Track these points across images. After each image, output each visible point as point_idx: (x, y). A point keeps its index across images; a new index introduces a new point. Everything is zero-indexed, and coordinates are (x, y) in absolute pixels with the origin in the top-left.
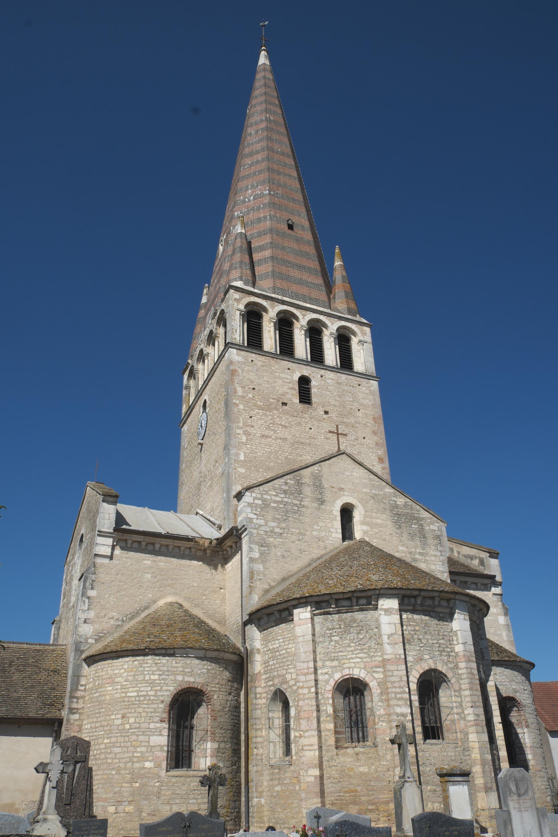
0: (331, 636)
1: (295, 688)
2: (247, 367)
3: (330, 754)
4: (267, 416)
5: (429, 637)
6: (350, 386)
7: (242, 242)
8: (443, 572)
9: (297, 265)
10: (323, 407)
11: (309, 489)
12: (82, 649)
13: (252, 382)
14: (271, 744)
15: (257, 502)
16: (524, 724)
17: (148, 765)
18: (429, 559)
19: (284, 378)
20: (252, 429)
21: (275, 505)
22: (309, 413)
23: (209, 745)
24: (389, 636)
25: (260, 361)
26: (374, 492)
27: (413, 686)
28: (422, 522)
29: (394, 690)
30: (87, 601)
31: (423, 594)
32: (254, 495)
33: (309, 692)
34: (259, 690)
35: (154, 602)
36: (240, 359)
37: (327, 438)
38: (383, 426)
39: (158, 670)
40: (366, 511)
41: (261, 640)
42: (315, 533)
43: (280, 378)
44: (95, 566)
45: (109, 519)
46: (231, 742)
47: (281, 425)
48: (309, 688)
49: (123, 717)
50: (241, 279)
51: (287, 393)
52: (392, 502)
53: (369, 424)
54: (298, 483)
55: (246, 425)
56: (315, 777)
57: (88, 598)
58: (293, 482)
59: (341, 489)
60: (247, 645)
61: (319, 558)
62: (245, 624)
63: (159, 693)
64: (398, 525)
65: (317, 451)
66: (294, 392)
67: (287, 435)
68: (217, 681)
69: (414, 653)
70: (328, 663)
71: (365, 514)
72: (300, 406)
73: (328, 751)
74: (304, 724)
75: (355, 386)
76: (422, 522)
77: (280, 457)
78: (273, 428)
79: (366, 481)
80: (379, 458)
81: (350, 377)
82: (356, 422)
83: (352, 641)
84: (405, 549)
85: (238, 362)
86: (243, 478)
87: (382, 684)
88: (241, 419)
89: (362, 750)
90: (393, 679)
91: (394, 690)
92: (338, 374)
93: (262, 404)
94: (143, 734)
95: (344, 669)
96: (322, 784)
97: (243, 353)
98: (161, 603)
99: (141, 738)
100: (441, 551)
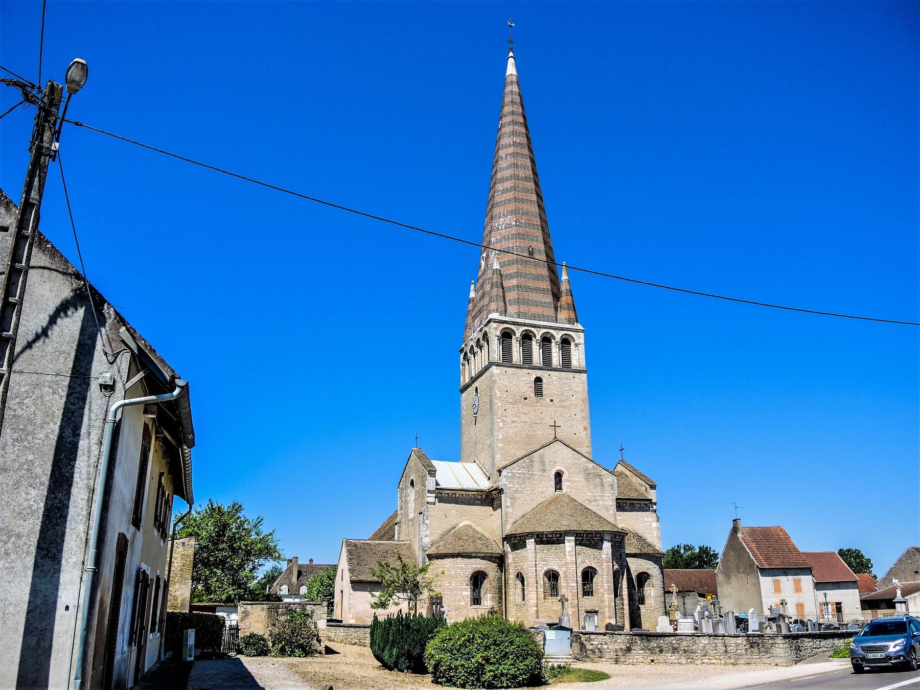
1: (527, 572)
3: (541, 602)
5: (589, 551)
11: (537, 464)
16: (651, 585)
17: (462, 603)
23: (488, 595)
24: (569, 552)
26: (574, 461)
27: (579, 574)
32: (507, 471)
33: (533, 575)
34: (511, 571)
35: (458, 525)
38: (588, 405)
42: (540, 489)
51: (527, 391)
56: (535, 611)
57: (426, 524)
59: (555, 462)
61: (542, 503)
64: (587, 480)
66: (531, 389)
69: (581, 559)
70: (541, 562)
72: (535, 399)
73: (540, 600)
74: (530, 589)
79: (570, 456)
84: (591, 494)
87: (565, 573)
96: (537, 613)
98: (461, 525)
99: (458, 592)
100: (612, 494)
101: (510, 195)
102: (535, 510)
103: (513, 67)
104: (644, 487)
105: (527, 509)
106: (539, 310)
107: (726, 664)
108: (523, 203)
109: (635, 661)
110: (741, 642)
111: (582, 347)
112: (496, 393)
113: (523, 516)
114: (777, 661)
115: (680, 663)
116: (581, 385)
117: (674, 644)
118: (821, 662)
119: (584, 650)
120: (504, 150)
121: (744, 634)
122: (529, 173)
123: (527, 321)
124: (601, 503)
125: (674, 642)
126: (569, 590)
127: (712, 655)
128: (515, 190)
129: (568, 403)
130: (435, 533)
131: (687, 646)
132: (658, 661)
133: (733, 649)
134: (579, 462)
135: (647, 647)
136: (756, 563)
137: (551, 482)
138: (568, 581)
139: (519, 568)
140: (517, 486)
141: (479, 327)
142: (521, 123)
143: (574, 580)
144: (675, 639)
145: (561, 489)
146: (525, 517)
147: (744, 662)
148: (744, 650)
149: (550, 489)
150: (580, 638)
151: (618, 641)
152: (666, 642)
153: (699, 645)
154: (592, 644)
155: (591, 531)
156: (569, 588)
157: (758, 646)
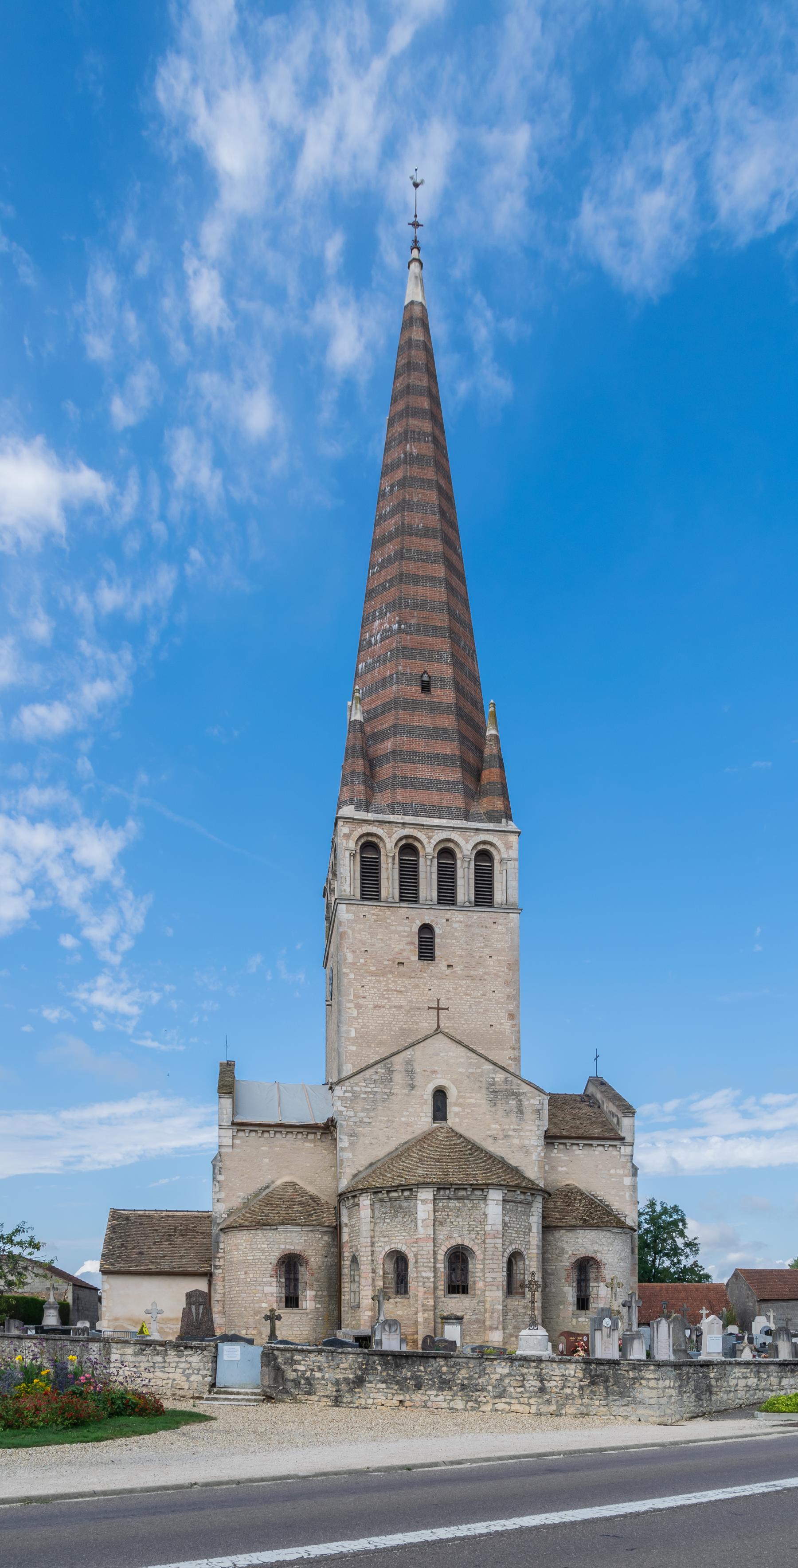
0: (385, 1218)
2: (359, 926)
4: (379, 982)
6: (482, 927)
7: (355, 738)
8: (538, 1146)
9: (428, 757)
10: (446, 960)
12: (218, 1222)
13: (364, 943)
14: (352, 1293)
15: (347, 1094)
18: (524, 1134)
19: (401, 931)
20: (364, 1000)
21: (365, 1096)
25: (374, 914)
26: (470, 1070)
27: (441, 1257)
28: (521, 1097)
29: (422, 1260)
30: (217, 1184)
32: (344, 1088)
35: (273, 1182)
36: (350, 916)
37: (448, 999)
39: (267, 1241)
40: (459, 1092)
42: (403, 1119)
43: (396, 932)
44: (220, 1156)
45: (227, 1114)
47: (396, 991)
49: (246, 1273)
50: (351, 802)
51: (404, 950)
52: (489, 1080)
53: (501, 974)
54: (389, 1071)
55: (357, 996)
56: (369, 1316)
57: (218, 1182)
58: (383, 1071)
59: (434, 1072)
61: (406, 1143)
63: (268, 1257)
66: (412, 947)
67: (403, 1002)
68: (313, 1248)
69: (445, 1233)
70: (382, 1239)
71: (458, 1096)
76: (521, 1097)
77: (394, 1028)
78: (386, 996)
79: (462, 1060)
80: (509, 1014)
81: (484, 914)
82: (485, 973)
83: (398, 1223)
85: (348, 920)
86: (354, 1056)
91: (422, 1260)
92: (469, 914)
93: (375, 969)
94: (259, 1285)
97: (353, 908)
98: (279, 1182)
99: (258, 1288)
100: (539, 1125)
105: (380, 1152)
106: (433, 797)
107: (539, 1414)
108: (416, 583)
109: (370, 1401)
111: (512, 866)
113: (371, 1165)
114: (642, 1411)
117: (444, 1374)
118: (741, 1418)
119: (281, 1381)
122: (434, 520)
123: (408, 819)
124: (516, 1141)
125: (444, 1369)
126: (421, 1284)
129: (481, 971)
130: (233, 1195)
131: (467, 1378)
132: (412, 1404)
133: (556, 1387)
134: (479, 1071)
135: (394, 1377)
137: (425, 1107)
138: (420, 1269)
140: (361, 1115)
142: (424, 411)
143: (430, 1267)
144: (446, 1365)
145: (444, 1118)
146: (374, 1167)
149: (423, 1119)
150: (276, 1359)
151: (342, 1366)
153: (492, 1376)
154: (295, 1370)
156: (421, 1279)
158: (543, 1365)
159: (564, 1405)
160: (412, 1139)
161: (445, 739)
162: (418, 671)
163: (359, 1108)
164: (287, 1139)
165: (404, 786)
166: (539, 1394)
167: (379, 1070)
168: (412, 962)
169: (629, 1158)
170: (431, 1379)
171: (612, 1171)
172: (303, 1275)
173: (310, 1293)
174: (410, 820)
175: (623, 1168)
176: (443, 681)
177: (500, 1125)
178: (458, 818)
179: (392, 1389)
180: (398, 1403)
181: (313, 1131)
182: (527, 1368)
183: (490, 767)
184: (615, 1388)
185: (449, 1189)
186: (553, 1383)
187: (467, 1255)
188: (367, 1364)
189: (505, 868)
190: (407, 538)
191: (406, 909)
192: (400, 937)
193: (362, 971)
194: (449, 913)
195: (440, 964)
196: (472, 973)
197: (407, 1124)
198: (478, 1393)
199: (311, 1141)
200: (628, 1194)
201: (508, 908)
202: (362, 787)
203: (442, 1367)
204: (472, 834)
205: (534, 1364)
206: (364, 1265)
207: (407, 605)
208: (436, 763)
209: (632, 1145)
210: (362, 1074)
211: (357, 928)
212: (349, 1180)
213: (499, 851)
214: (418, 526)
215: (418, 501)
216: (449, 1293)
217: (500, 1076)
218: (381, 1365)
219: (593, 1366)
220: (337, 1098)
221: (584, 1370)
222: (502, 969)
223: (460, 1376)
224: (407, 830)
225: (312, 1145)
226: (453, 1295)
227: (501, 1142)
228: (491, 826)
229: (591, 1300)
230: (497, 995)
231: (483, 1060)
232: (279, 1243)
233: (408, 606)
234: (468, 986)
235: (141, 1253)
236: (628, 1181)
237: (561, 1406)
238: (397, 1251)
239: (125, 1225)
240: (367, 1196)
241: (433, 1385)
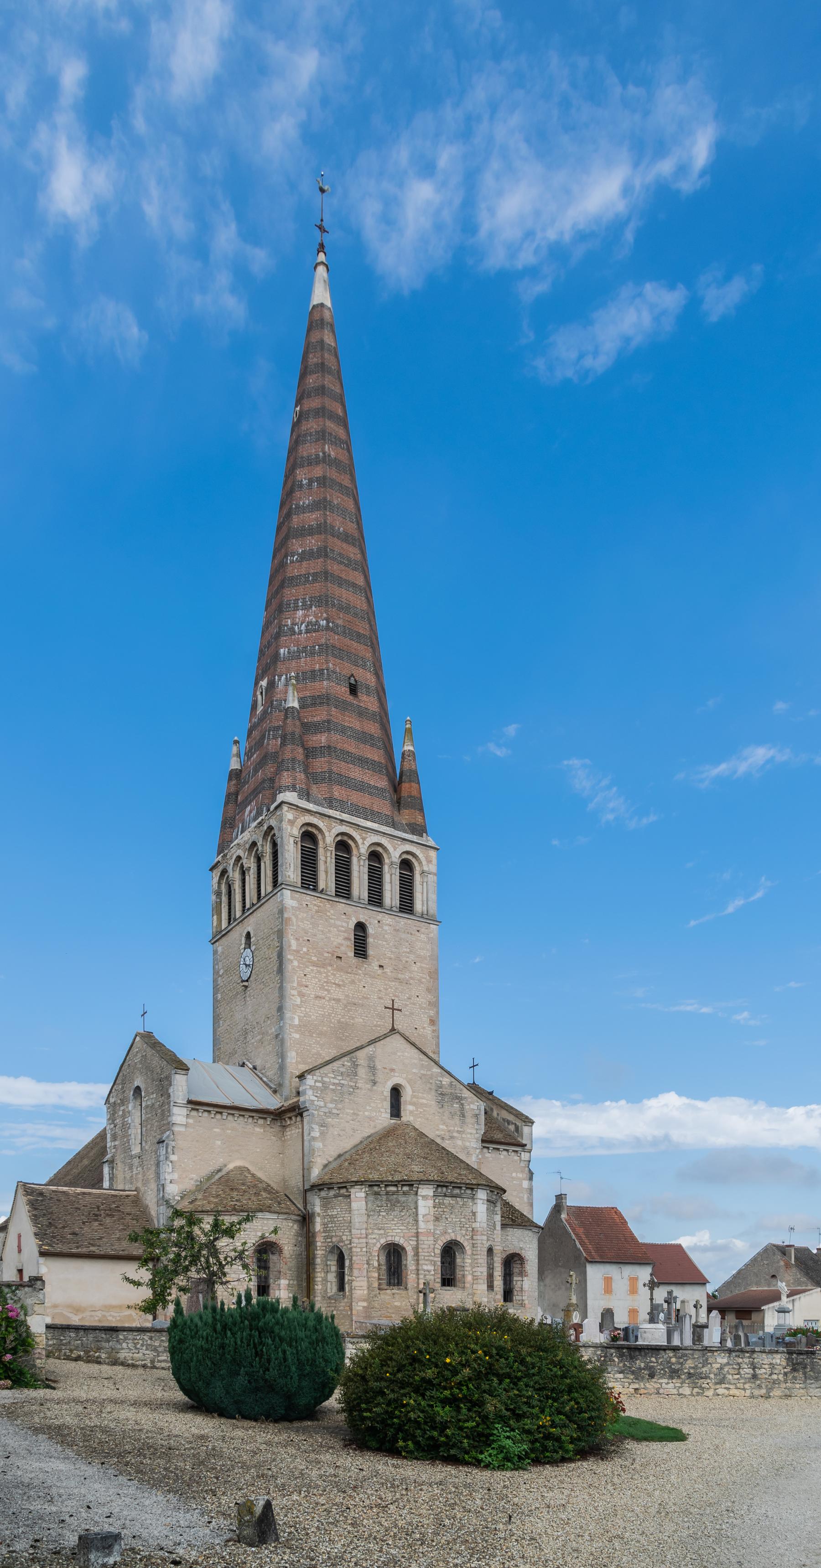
0: (380, 1211)
1: (349, 1246)
3: (374, 1293)
8: (477, 1148)
9: (359, 759)
19: (340, 926)
20: (306, 989)
22: (364, 969)
26: (422, 1072)
30: (170, 1164)
31: (453, 1185)
32: (315, 1078)
34: (319, 1244)
35: (225, 1166)
37: (380, 998)
40: (413, 1092)
41: (321, 1206)
42: (366, 1113)
46: (297, 1280)
47: (335, 984)
48: (361, 1248)
51: (342, 945)
53: (423, 980)
54: (354, 1065)
55: (300, 984)
56: (364, 1307)
58: (349, 1064)
59: (392, 1070)
60: (308, 1207)
61: (369, 1137)
62: (306, 1191)
64: (441, 1104)
65: (370, 1013)
68: (286, 1236)
70: (376, 1231)
72: (355, 961)
74: (356, 1272)
75: (413, 933)
77: (333, 1020)
78: (326, 988)
79: (416, 1061)
80: (430, 1020)
81: (409, 922)
82: (411, 978)
83: (395, 1217)
86: (297, 1044)
87: (416, 1249)
88: (296, 978)
89: (397, 1291)
90: (423, 1246)
92: (397, 918)
93: (316, 959)
95: (388, 1236)
97: (297, 895)
98: (231, 1166)
100: (477, 1129)
101: (315, 566)
102: (359, 1147)
103: (325, 289)
104: (514, 1126)
105: (347, 1144)
106: (364, 800)
107: (752, 1396)
108: (340, 585)
110: (778, 1361)
111: (432, 879)
112: (290, 942)
113: (340, 1156)
115: (682, 1394)
116: (429, 947)
117: (673, 1364)
120: (306, 470)
121: (785, 1350)
123: (345, 817)
124: (459, 1143)
125: (673, 1360)
127: (733, 1382)
128: (326, 556)
129: (407, 976)
130: (186, 1177)
132: (646, 1391)
133: (765, 1373)
134: (429, 1073)
136: (585, 1254)
139: (334, 1239)
141: (255, 819)
144: (675, 1356)
146: (343, 1158)
147: (780, 1394)
148: (782, 1375)
152: (661, 1360)
155: (460, 1183)
157: (805, 1368)
158: (755, 1356)
159: (772, 1389)
160: (374, 1134)
161: (372, 745)
162: (346, 672)
163: (328, 1099)
164: (238, 1122)
165: (340, 784)
166: (752, 1380)
167: (346, 1063)
168: (348, 957)
169: (527, 1163)
170: (662, 1369)
171: (514, 1175)
172: (275, 1263)
173: (284, 1282)
174: (346, 818)
175: (522, 1172)
176: (368, 687)
177: (447, 1126)
178: (387, 824)
179: (628, 1378)
180: (632, 1391)
181: (265, 1116)
182: (742, 1358)
183: (410, 781)
184: (812, 1373)
185: (446, 1187)
186: (763, 1371)
187: (455, 1249)
188: (605, 1357)
189: (425, 880)
190: (331, 539)
191: (343, 905)
192: (338, 931)
193: (305, 960)
194: (381, 915)
195: (373, 965)
196: (400, 976)
197: (370, 1118)
198: (702, 1380)
199: (261, 1126)
200: (526, 1196)
201: (427, 918)
202: (303, 776)
203: (671, 1358)
204: (399, 843)
205: (747, 1355)
206: (357, 1256)
207: (333, 605)
208: (366, 767)
209: (530, 1151)
210: (331, 1065)
211: (300, 917)
212: (320, 1169)
213: (420, 863)
214: (339, 529)
215: (338, 504)
216: (389, 1284)
217: (446, 1080)
218: (618, 1357)
219: (795, 1356)
220: (308, 1087)
221: (788, 1359)
222: (424, 976)
223: (687, 1366)
224: (344, 827)
225: (262, 1130)
226: (448, 1288)
227: (447, 1142)
228: (414, 838)
229: (515, 1293)
230: (420, 1000)
231: (433, 1064)
232: (256, 1231)
233: (335, 606)
234: (396, 988)
235: (74, 1234)
236: (526, 1184)
237: (769, 1390)
238: (394, 1244)
239: (42, 1201)
240: (362, 1189)
241: (664, 1375)
